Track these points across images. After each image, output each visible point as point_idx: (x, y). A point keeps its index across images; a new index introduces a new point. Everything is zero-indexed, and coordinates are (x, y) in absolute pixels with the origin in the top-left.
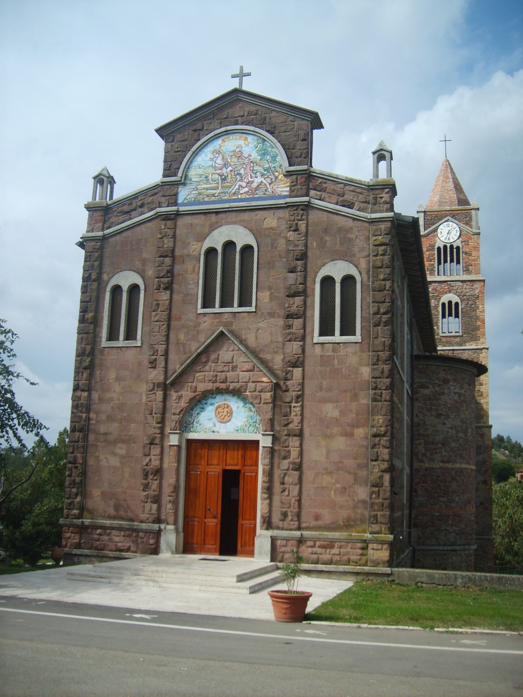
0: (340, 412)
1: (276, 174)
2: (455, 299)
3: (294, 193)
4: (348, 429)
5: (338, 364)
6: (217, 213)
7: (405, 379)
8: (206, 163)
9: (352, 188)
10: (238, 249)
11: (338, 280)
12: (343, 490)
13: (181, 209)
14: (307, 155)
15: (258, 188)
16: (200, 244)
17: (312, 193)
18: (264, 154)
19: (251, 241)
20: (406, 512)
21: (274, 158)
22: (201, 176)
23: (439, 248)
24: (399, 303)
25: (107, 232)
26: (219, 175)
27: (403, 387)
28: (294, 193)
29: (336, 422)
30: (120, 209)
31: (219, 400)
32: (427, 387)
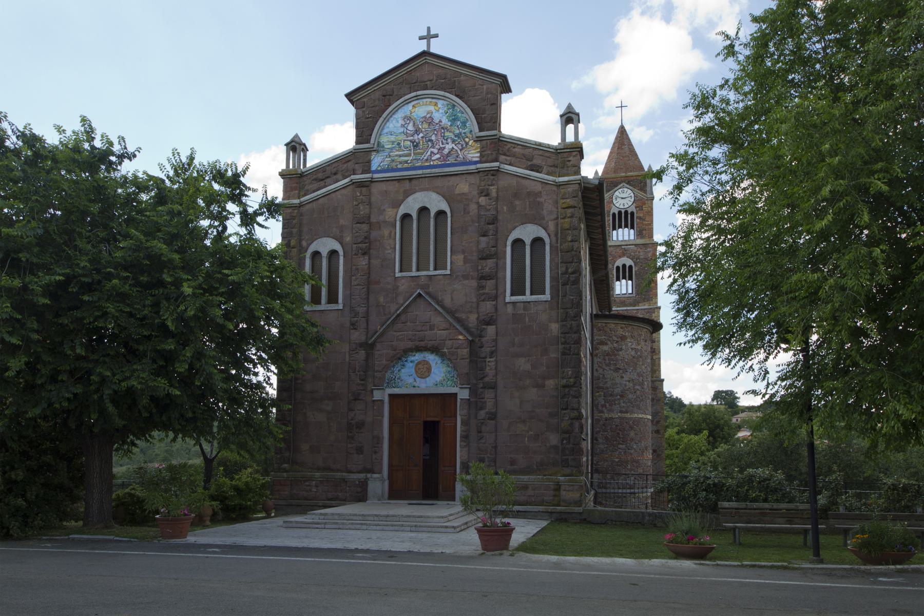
1: (467, 140)
2: (629, 262)
3: (484, 159)
6: (410, 180)
7: (587, 336)
8: (394, 127)
9: (541, 153)
10: (432, 214)
13: (376, 176)
14: (495, 121)
15: (449, 154)
16: (395, 210)
17: (502, 158)
18: (454, 119)
19: (444, 206)
21: (464, 124)
22: (393, 142)
23: (614, 215)
25: (302, 199)
26: (411, 141)
28: (484, 159)
30: (315, 177)
31: (418, 357)
32: (606, 344)
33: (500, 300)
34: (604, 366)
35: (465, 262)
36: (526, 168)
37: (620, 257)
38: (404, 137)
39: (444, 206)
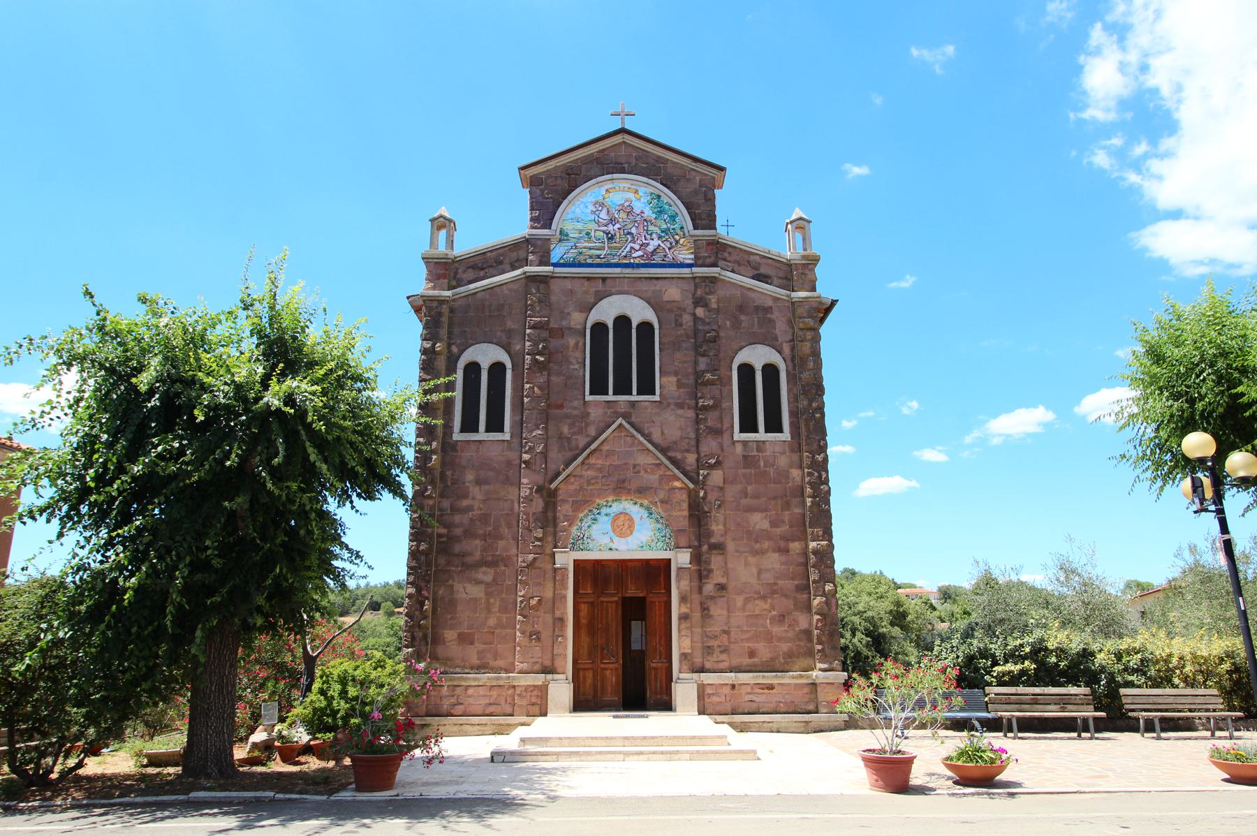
0: (771, 522)
3: (700, 262)
4: (782, 544)
5: (765, 466)
12: (781, 618)
17: (721, 263)
19: (650, 316)
22: (580, 231)
29: (766, 535)
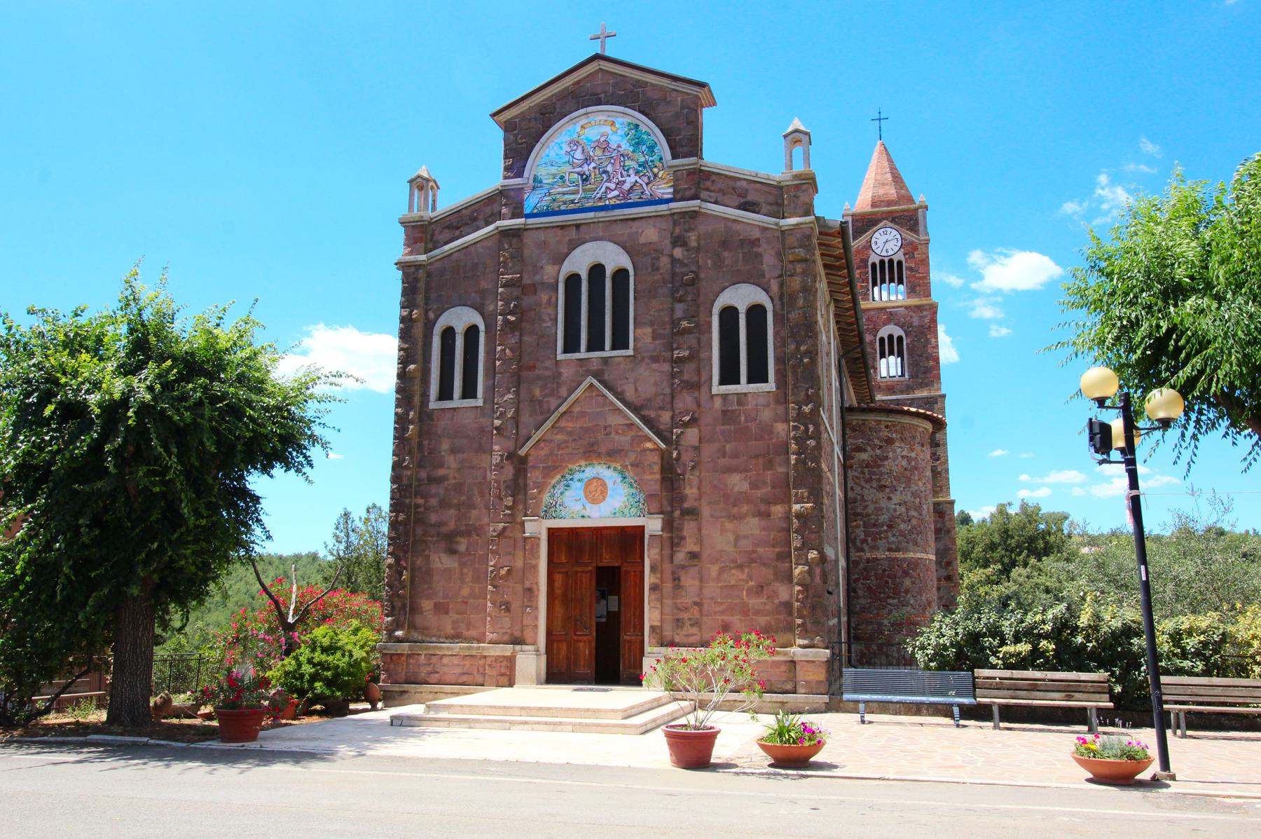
1: (655, 170)
2: (897, 332)
3: (679, 196)
4: (763, 507)
5: (746, 421)
6: (578, 226)
7: (834, 440)
8: (555, 154)
11: (742, 310)
16: (556, 267)
17: (704, 194)
18: (638, 143)
19: (625, 262)
20: (844, 619)
21: (651, 148)
22: (554, 176)
23: (874, 265)
24: (824, 338)
27: (833, 451)
29: (745, 498)
32: (865, 450)
33: (704, 389)
34: (863, 483)
35: (654, 339)
36: (739, 208)
37: (885, 324)
38: (570, 168)
39: (625, 262)
